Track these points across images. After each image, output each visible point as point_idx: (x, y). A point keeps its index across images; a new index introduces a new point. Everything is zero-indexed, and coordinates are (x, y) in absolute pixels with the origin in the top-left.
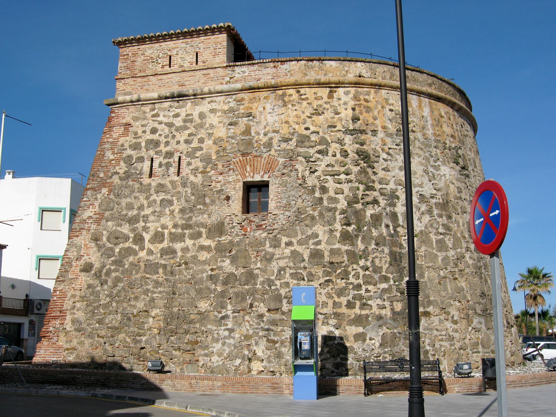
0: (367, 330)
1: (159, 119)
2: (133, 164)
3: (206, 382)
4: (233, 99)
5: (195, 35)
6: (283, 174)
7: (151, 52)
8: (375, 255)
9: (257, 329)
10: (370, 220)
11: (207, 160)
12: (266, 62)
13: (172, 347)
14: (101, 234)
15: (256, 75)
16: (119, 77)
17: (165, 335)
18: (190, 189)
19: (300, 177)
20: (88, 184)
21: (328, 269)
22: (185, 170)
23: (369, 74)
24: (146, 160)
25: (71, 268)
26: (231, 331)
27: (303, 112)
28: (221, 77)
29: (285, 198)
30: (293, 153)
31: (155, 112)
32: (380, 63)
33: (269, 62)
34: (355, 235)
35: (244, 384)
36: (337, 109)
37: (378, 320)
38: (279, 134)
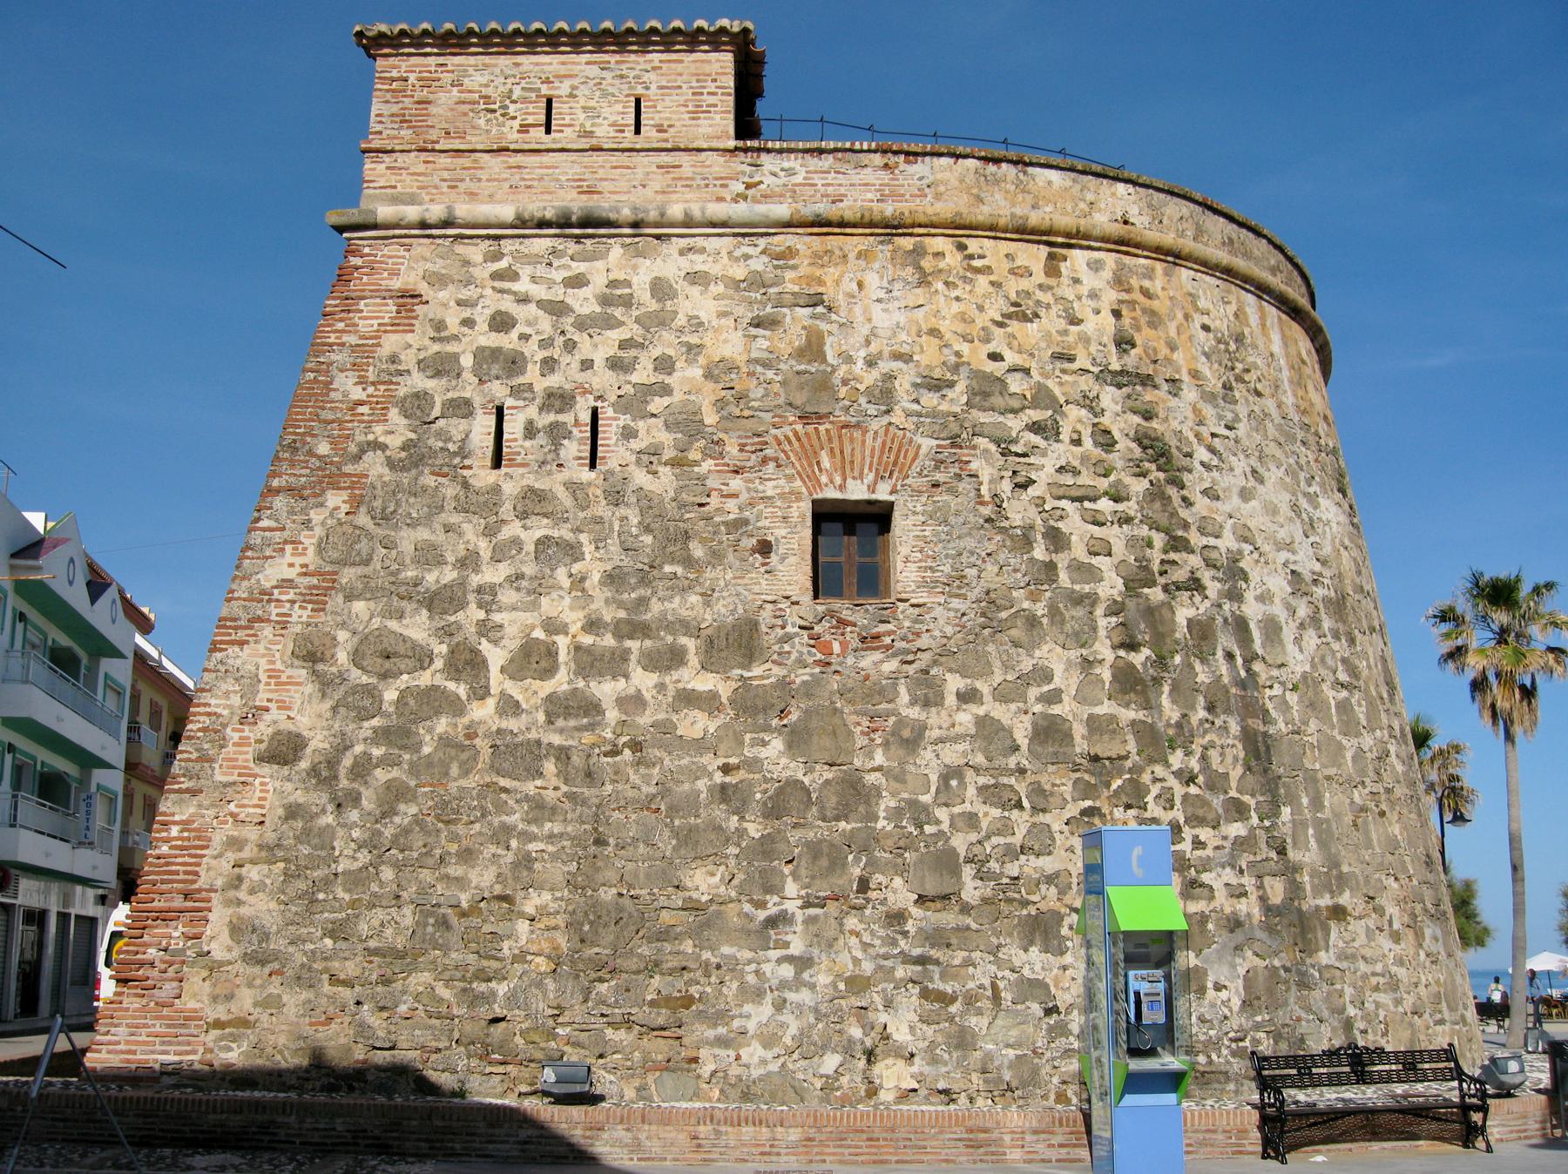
0: (1206, 961)
1: (516, 286)
2: (433, 422)
3: (748, 1131)
4: (759, 249)
5: (632, 44)
6: (934, 486)
7: (484, 80)
8: (1208, 738)
9: (886, 957)
10: (1188, 636)
11: (687, 424)
12: (861, 151)
13: (603, 1015)
14: (327, 641)
15: (828, 185)
16: (376, 144)
17: (577, 976)
18: (637, 511)
19: (987, 498)
20: (274, 475)
21: (1087, 777)
22: (615, 452)
23: (1146, 220)
24: (479, 412)
25: (222, 747)
26: (802, 963)
27: (981, 308)
28: (716, 179)
29: (947, 556)
30: (962, 426)
31: (504, 264)
32: (1172, 193)
33: (869, 151)
34: (1154, 679)
35: (875, 1135)
36: (1073, 308)
37: (1232, 931)
38: (911, 364)
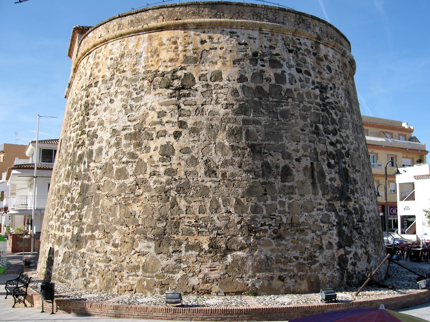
32: (111, 20)
